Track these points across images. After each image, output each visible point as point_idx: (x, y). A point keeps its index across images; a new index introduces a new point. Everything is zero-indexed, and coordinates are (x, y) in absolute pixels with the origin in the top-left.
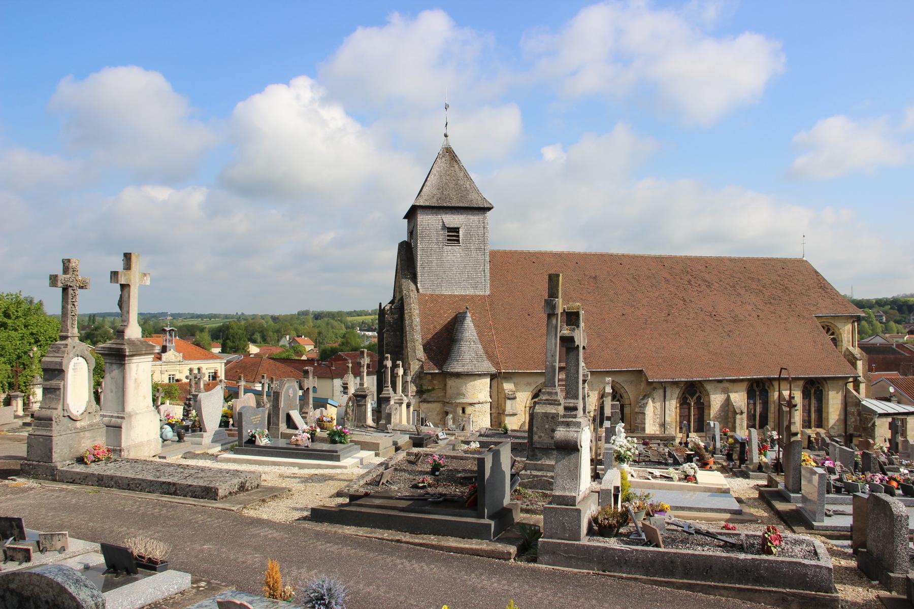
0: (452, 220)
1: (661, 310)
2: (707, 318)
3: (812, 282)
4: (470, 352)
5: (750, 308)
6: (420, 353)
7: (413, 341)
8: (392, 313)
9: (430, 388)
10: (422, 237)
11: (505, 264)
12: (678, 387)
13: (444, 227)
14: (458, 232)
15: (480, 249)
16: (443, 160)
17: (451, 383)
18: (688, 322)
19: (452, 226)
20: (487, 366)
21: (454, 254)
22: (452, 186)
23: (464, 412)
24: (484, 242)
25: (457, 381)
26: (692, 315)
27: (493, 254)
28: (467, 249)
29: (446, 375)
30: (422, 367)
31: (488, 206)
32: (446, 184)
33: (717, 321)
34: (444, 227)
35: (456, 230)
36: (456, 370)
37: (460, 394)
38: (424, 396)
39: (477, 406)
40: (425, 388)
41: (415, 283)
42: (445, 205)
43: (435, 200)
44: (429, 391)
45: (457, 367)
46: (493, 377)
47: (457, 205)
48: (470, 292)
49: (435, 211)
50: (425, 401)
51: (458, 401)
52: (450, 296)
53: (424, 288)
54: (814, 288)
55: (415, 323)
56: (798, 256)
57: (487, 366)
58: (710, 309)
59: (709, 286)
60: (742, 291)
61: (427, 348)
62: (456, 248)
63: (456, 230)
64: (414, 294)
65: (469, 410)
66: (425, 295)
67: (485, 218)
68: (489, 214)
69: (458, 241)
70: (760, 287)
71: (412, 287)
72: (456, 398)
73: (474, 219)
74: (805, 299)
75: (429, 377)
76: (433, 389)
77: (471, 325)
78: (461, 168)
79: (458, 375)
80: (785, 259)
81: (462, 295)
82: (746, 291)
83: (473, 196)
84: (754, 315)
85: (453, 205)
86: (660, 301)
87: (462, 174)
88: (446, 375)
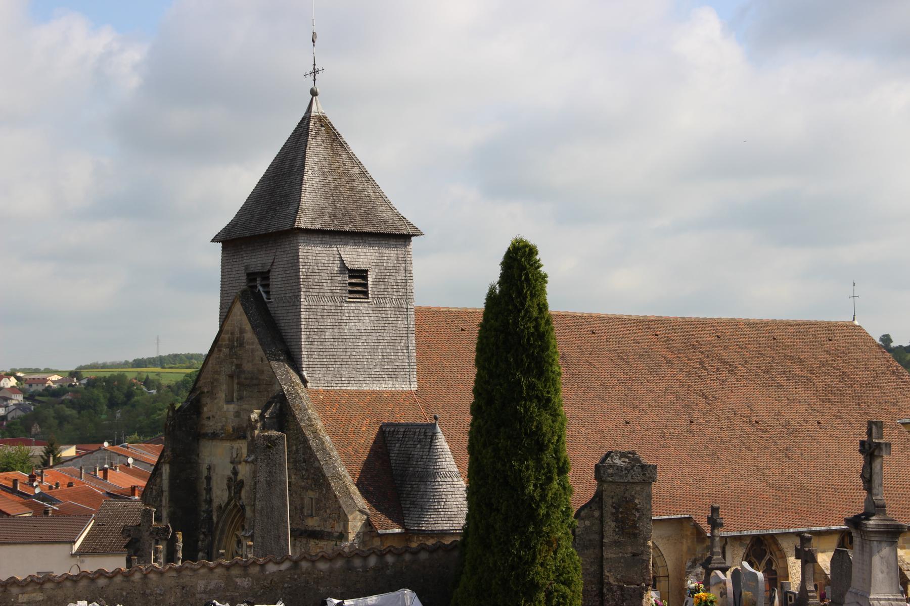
0: (358, 256)
1: (678, 414)
2: (747, 427)
3: (878, 363)
5: (802, 408)
6: (361, 501)
7: (339, 477)
10: (308, 287)
12: (741, 545)
13: (343, 267)
14: (365, 278)
18: (723, 434)
21: (359, 316)
24: (406, 295)
26: (725, 423)
28: (379, 308)
30: (368, 524)
31: (415, 232)
33: (764, 431)
36: (439, 527)
41: (299, 371)
42: (347, 229)
47: (365, 229)
48: (387, 386)
54: (884, 373)
56: (844, 317)
58: (747, 412)
59: (731, 372)
60: (782, 380)
62: (363, 307)
63: (362, 274)
64: (301, 388)
68: (568, 289)
69: (366, 293)
70: (805, 373)
71: (296, 378)
73: (390, 253)
74: (877, 393)
77: (447, 447)
78: (352, 158)
80: (829, 323)
81: (374, 392)
82: (788, 379)
84: (812, 420)
85: (359, 229)
86: (671, 397)
87: (356, 171)
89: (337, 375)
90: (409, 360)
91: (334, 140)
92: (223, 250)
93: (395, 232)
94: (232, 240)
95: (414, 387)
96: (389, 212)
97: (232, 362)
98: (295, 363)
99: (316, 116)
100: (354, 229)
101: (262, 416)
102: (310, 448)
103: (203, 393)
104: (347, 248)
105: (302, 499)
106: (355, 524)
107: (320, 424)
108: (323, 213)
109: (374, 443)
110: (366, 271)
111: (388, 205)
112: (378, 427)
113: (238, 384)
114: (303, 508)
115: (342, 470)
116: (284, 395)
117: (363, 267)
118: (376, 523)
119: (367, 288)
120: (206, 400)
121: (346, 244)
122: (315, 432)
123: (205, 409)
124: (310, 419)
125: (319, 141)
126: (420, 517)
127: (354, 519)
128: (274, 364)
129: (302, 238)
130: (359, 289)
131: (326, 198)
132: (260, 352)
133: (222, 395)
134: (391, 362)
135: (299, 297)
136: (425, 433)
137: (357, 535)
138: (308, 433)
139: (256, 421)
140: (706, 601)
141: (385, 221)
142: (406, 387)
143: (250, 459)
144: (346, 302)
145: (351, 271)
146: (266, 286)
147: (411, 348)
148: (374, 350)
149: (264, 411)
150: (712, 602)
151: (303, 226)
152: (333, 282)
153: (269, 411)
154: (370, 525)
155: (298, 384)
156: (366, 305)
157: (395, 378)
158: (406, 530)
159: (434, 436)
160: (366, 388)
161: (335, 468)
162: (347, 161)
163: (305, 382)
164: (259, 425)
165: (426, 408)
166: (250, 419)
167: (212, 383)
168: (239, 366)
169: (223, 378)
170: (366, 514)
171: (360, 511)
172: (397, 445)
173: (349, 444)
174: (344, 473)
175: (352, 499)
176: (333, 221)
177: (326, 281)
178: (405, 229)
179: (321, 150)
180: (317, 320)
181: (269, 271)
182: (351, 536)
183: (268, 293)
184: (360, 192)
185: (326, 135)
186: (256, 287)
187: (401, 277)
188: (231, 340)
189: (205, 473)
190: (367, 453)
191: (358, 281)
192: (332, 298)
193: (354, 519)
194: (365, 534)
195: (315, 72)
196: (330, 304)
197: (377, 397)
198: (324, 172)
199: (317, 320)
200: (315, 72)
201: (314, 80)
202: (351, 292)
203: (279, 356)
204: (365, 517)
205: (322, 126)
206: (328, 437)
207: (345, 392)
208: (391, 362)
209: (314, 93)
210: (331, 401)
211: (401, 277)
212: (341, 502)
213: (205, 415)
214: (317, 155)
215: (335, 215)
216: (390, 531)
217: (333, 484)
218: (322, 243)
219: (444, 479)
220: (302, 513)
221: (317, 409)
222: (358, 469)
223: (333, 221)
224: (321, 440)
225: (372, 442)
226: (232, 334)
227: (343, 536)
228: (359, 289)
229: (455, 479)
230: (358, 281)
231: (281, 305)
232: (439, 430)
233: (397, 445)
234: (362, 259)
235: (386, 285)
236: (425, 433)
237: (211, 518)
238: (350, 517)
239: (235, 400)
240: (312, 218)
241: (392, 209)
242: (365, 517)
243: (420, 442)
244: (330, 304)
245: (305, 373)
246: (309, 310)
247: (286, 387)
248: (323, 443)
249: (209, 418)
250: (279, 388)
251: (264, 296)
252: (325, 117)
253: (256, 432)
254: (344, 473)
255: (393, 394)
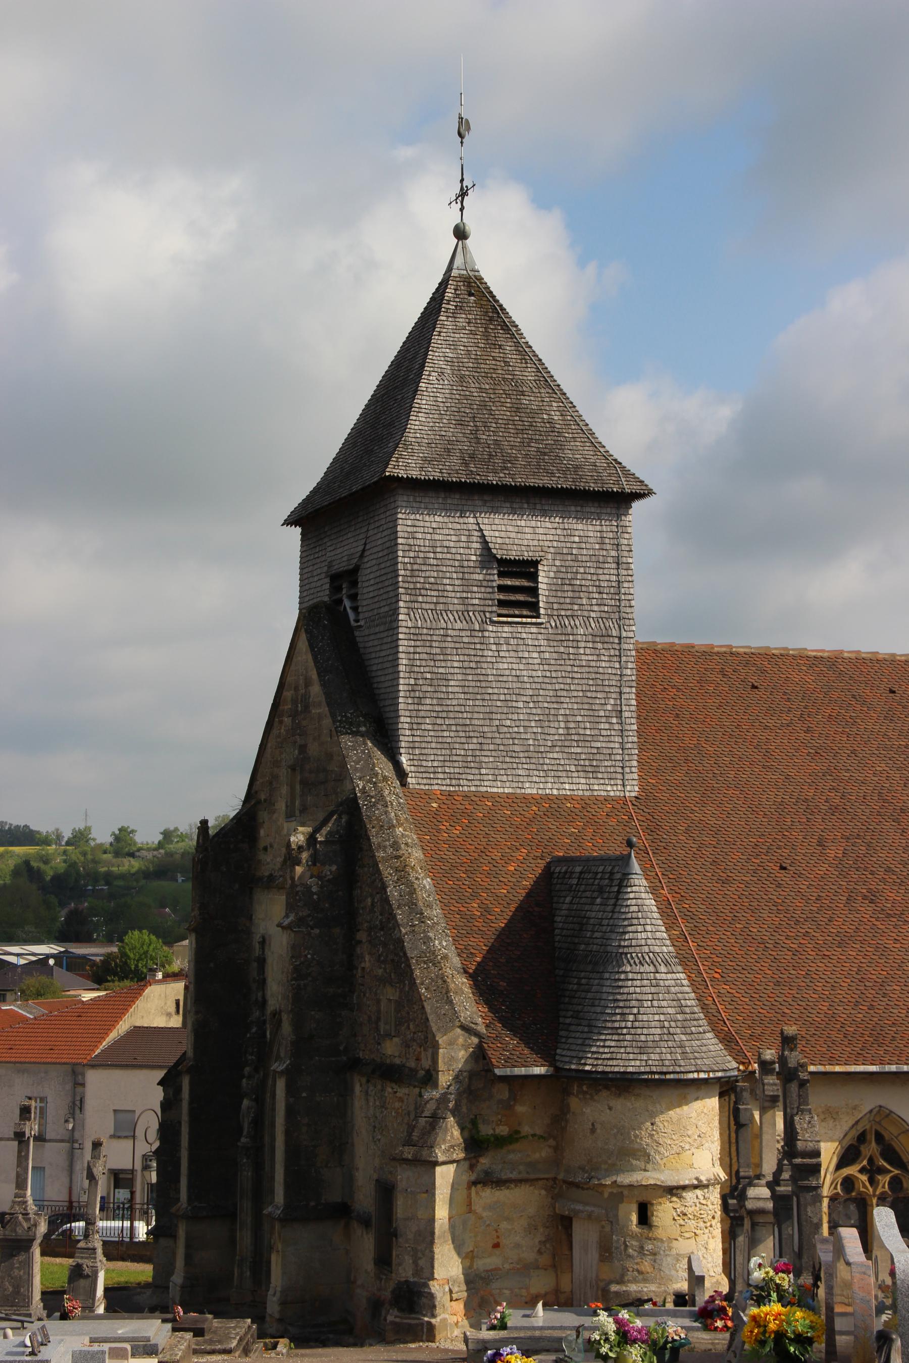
0: (517, 533)
4: (661, 1000)
6: (468, 1005)
7: (432, 959)
8: (314, 859)
9: (503, 1130)
10: (414, 592)
11: (704, 697)
13: (488, 557)
14: (534, 577)
15: (605, 636)
16: (462, 320)
17: (594, 1112)
19: (513, 555)
20: (712, 1056)
21: (519, 652)
22: (503, 413)
23: (644, 1218)
24: (618, 610)
25: (619, 1104)
27: (653, 658)
28: (562, 636)
29: (567, 1084)
30: (480, 1055)
31: (636, 488)
32: (483, 405)
34: (488, 557)
35: (526, 569)
37: (633, 1154)
38: (485, 1162)
39: (689, 1196)
40: (486, 1130)
41: (392, 755)
42: (493, 479)
43: (455, 461)
44: (500, 1142)
45: (611, 1055)
46: (727, 1089)
47: (533, 482)
48: (574, 786)
49: (455, 499)
50: (487, 1180)
51: (625, 1179)
52: (511, 799)
53: (422, 771)
55: (422, 895)
57: (712, 1056)
61: (484, 982)
63: (526, 569)
64: (392, 791)
65: (664, 1212)
66: (427, 795)
67: (622, 530)
69: (533, 607)
71: (384, 767)
72: (615, 1169)
73: (586, 531)
75: (502, 1092)
76: (514, 1137)
77: (650, 903)
78: (525, 353)
79: (625, 1084)
83: (575, 452)
85: (520, 480)
87: (530, 375)
88: (567, 1084)
89: (472, 763)
90: (621, 738)
91: (491, 319)
92: (302, 540)
93: (593, 486)
94: (316, 518)
95: (632, 790)
96: (588, 451)
97: (295, 742)
98: (386, 738)
99: (460, 276)
100: (509, 481)
101: (311, 839)
102: (386, 900)
103: (259, 802)
104: (497, 519)
105: (378, 1002)
106: (453, 1056)
107: (416, 855)
108: (449, 450)
109: (528, 895)
110: (535, 564)
111: (588, 436)
112: (542, 864)
113: (301, 782)
114: (379, 1019)
115: (443, 945)
116: (355, 798)
117: (527, 555)
118: (493, 1055)
119: (536, 595)
120: (263, 815)
121: (495, 510)
122: (402, 871)
123: (262, 832)
124: (396, 846)
125: (462, 320)
126: (585, 1044)
127: (451, 1043)
128: (347, 741)
129: (402, 499)
130: (521, 597)
131: (460, 423)
132: (327, 722)
133: (281, 806)
134: (583, 740)
135: (395, 612)
136: (612, 873)
137: (456, 1078)
138: (387, 872)
139: (300, 848)
140: (780, 1336)
141: (577, 468)
142: (613, 791)
143: (286, 922)
144: (493, 622)
145: (502, 562)
146: (353, 597)
147: (626, 714)
148: (547, 717)
149: (317, 830)
150: (802, 1340)
151: (402, 474)
152: (467, 584)
153: (325, 830)
154: (484, 1058)
155: (385, 779)
156: (534, 630)
157: (592, 771)
158: (557, 1069)
159: (623, 881)
160: (530, 790)
161: (427, 940)
162: (513, 357)
163: (402, 775)
164: (305, 856)
165: (650, 831)
166: (289, 844)
167: (271, 783)
168: (303, 748)
169: (283, 773)
170: (477, 1034)
171: (463, 1028)
172: (568, 899)
173: (475, 896)
174: (445, 954)
175: (450, 1002)
176: (466, 465)
177: (451, 582)
178: (618, 482)
179: (463, 338)
180: (432, 658)
181: (356, 570)
182: (445, 1079)
183: (355, 609)
184: (533, 414)
185: (477, 311)
186: (340, 601)
187: (608, 575)
188: (294, 702)
189: (257, 952)
190: (508, 914)
191: (517, 582)
192: (464, 616)
193: (451, 1043)
194: (472, 1075)
195: (463, 194)
196: (458, 625)
197: (553, 807)
198: (462, 377)
199: (432, 658)
200: (463, 194)
201: (462, 209)
202: (502, 604)
203: (359, 726)
204: (475, 1040)
205: (471, 294)
206: (427, 882)
207: (485, 796)
208: (583, 740)
209: (460, 234)
210: (453, 816)
211: (608, 575)
212: (428, 1008)
213: (262, 844)
214: (453, 346)
215: (472, 456)
216: (522, 1071)
217: (417, 973)
218: (447, 509)
219: (637, 968)
220: (377, 1029)
221: (418, 826)
222: (480, 947)
223: (466, 465)
224: (410, 885)
225: (523, 893)
226: (296, 689)
227: (430, 1078)
228: (521, 597)
229: (663, 969)
230: (517, 582)
231: (372, 631)
232: (636, 867)
233: (568, 899)
234: (528, 539)
235: (577, 591)
236: (612, 873)
237: (265, 1036)
238: (442, 1040)
239: (297, 813)
240: (425, 459)
241: (596, 445)
242: (475, 1040)
243: (601, 890)
244: (458, 625)
245: (404, 759)
246: (415, 636)
247: (361, 784)
248: (413, 892)
249: (265, 849)
250: (349, 787)
251: (352, 616)
252: (480, 279)
253: (299, 870)
254: (445, 954)
255: (586, 804)
